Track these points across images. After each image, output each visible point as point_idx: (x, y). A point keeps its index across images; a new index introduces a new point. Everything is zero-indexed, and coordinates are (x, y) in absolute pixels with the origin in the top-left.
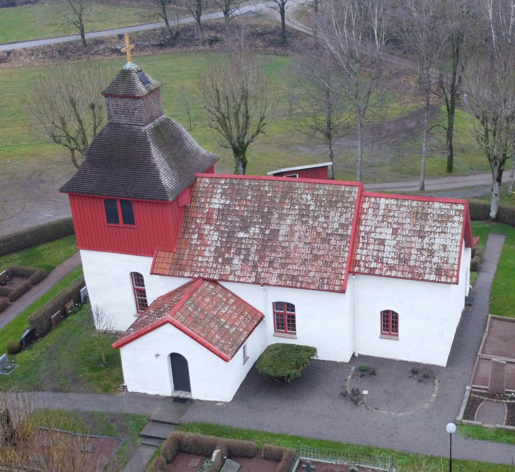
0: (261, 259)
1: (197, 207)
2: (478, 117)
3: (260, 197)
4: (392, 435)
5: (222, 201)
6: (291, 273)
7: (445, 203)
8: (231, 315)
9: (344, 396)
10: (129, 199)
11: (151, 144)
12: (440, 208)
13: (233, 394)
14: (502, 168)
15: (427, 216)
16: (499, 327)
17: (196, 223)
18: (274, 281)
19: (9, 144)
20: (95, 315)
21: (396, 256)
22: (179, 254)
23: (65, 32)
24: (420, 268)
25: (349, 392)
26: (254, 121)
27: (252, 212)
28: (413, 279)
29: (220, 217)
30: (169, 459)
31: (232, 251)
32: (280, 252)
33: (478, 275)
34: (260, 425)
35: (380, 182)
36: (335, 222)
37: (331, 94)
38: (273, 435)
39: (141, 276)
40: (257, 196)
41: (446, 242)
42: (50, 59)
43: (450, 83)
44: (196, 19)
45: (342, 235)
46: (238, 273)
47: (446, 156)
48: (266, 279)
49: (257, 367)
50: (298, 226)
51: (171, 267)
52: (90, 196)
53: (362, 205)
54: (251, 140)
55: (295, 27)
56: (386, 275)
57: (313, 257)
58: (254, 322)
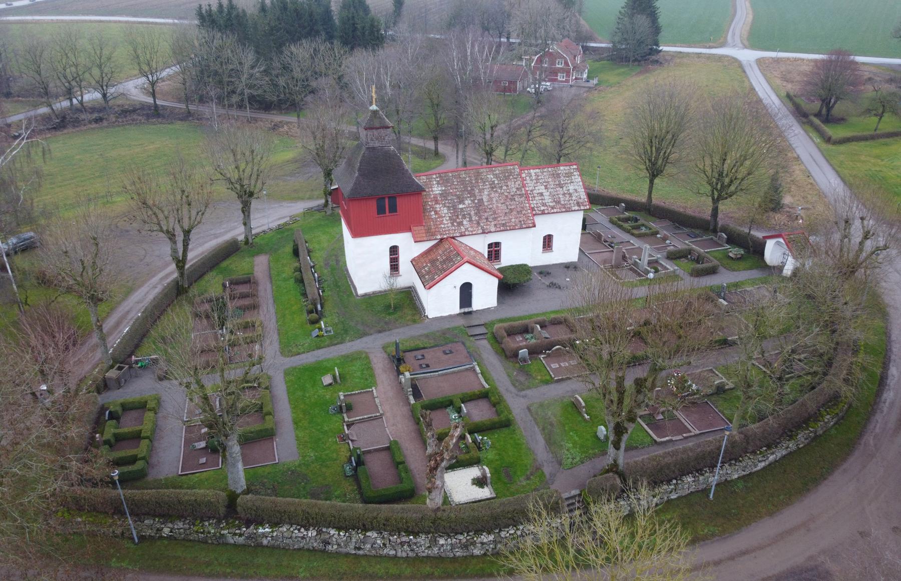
0: (480, 217)
5: (440, 189)
28: (566, 211)
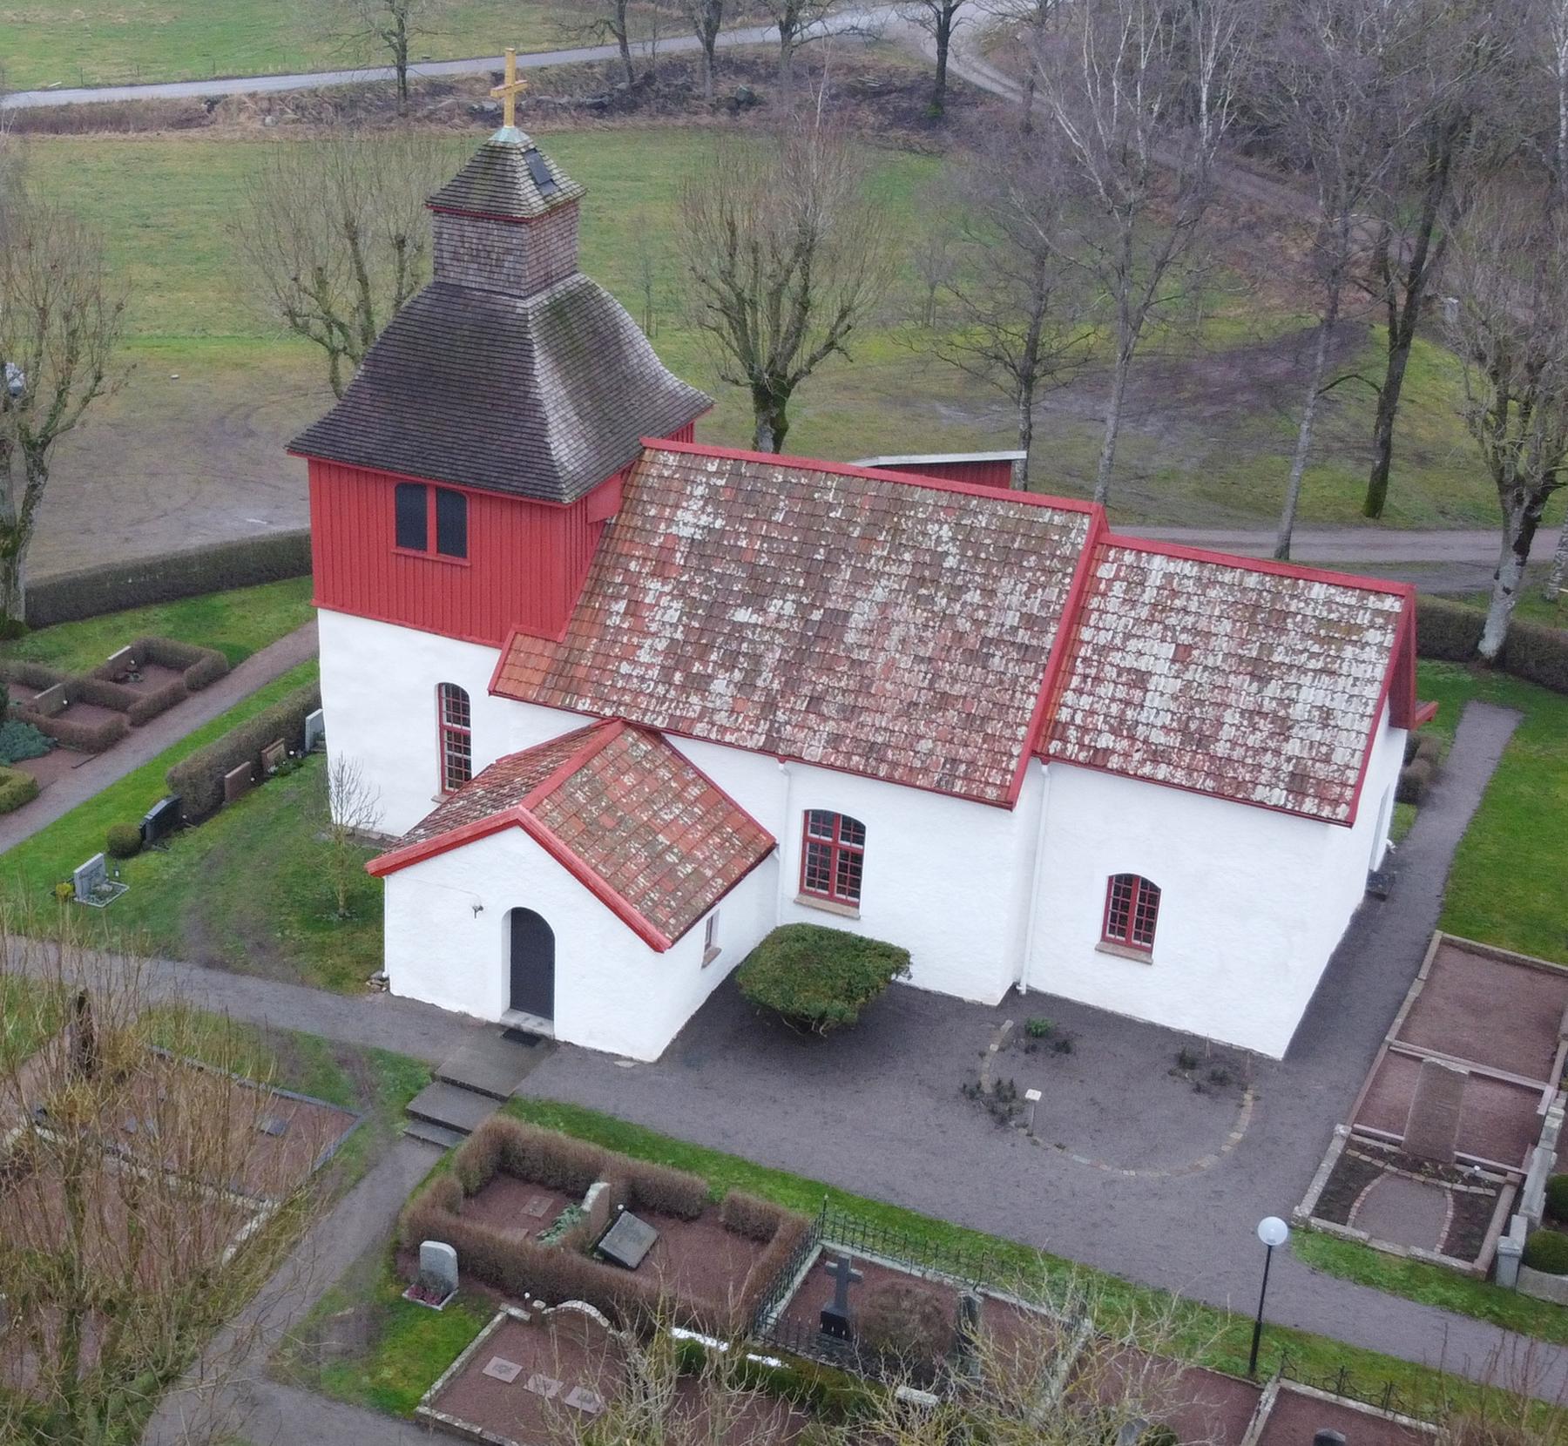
0: (791, 686)
1: (635, 528)
2: (1481, 358)
3: (810, 520)
4: (1095, 1225)
5: (704, 521)
6: (866, 734)
7: (1346, 587)
8: (687, 829)
9: (972, 1096)
10: (460, 488)
11: (536, 347)
12: (1328, 602)
13: (666, 1042)
14: (1536, 514)
15: (1285, 620)
16: (1465, 973)
17: (627, 570)
18: (815, 751)
19: (182, 331)
20: (332, 783)
21: (1175, 724)
22: (571, 649)
23: (358, 59)
24: (1244, 765)
25: (988, 1089)
26: (820, 325)
27: (784, 556)
28: (1217, 794)
29: (694, 562)
30: (473, 1189)
31: (714, 657)
32: (843, 673)
33: (1418, 814)
34: (725, 1135)
35: (1160, 524)
36: (1009, 608)
37: (1049, 261)
38: (756, 1170)
39: (465, 696)
40: (800, 514)
41: (1332, 699)
42: (312, 126)
43: (1407, 258)
44: (702, 40)
45: (1027, 647)
46: (721, 718)
47: (1368, 469)
48: (795, 742)
49: (740, 979)
50: (905, 608)
51: (544, 681)
52: (362, 470)
53: (1096, 570)
54: (805, 369)
55: (974, 78)
56: (1140, 772)
57: (934, 697)
58: (747, 858)
